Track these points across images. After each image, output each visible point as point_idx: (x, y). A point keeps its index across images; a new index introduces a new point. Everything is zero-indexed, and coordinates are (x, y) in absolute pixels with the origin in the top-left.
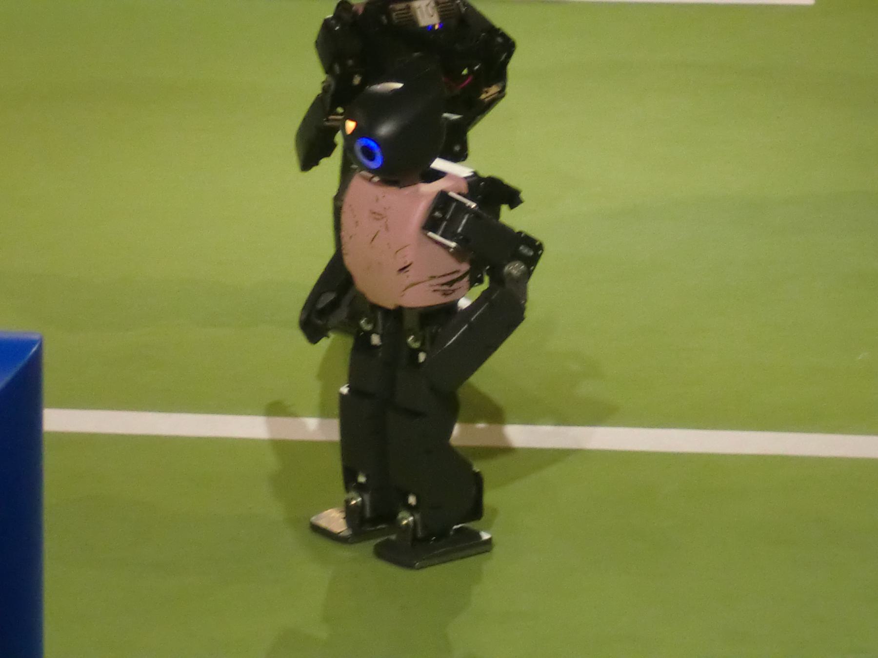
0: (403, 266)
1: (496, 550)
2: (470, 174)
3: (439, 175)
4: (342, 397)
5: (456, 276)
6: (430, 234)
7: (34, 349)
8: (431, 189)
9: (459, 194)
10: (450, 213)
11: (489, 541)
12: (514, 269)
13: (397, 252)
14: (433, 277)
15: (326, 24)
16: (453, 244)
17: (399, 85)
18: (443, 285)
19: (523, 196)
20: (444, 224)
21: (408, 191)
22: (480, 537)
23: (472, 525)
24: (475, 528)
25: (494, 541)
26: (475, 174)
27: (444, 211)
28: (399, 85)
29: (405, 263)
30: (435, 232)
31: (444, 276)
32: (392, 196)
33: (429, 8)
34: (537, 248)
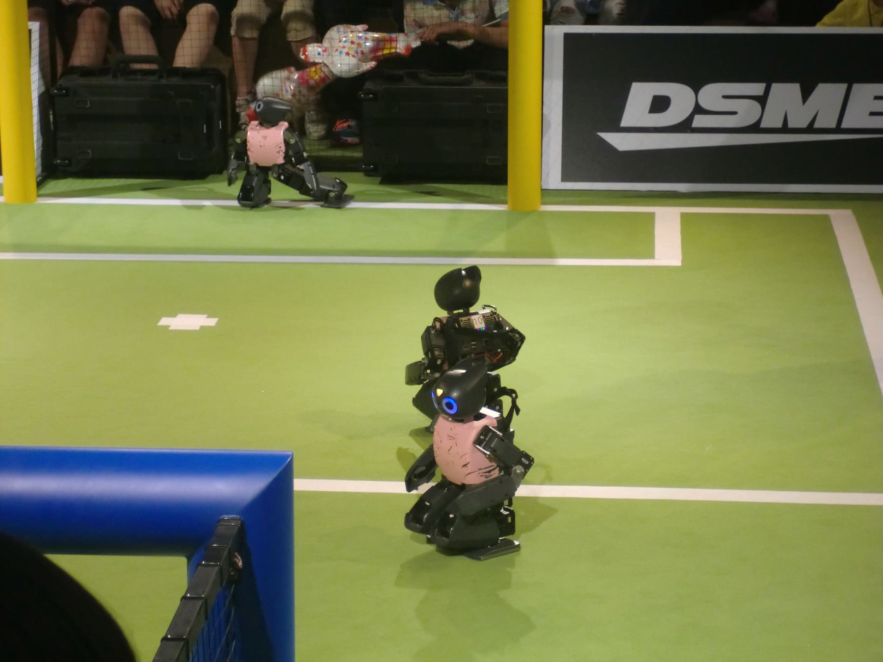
0: (465, 464)
1: (522, 550)
3: (483, 416)
5: (491, 468)
6: (477, 446)
8: (479, 424)
9: (493, 427)
10: (489, 437)
11: (518, 546)
12: (519, 469)
14: (480, 469)
15: (428, 330)
16: (488, 453)
17: (464, 371)
18: (485, 473)
20: (485, 442)
21: (466, 425)
22: (514, 543)
23: (509, 537)
24: (511, 539)
25: (521, 546)
27: (486, 436)
28: (464, 371)
29: (466, 462)
30: (480, 446)
31: (486, 468)
32: (459, 427)
34: (531, 460)
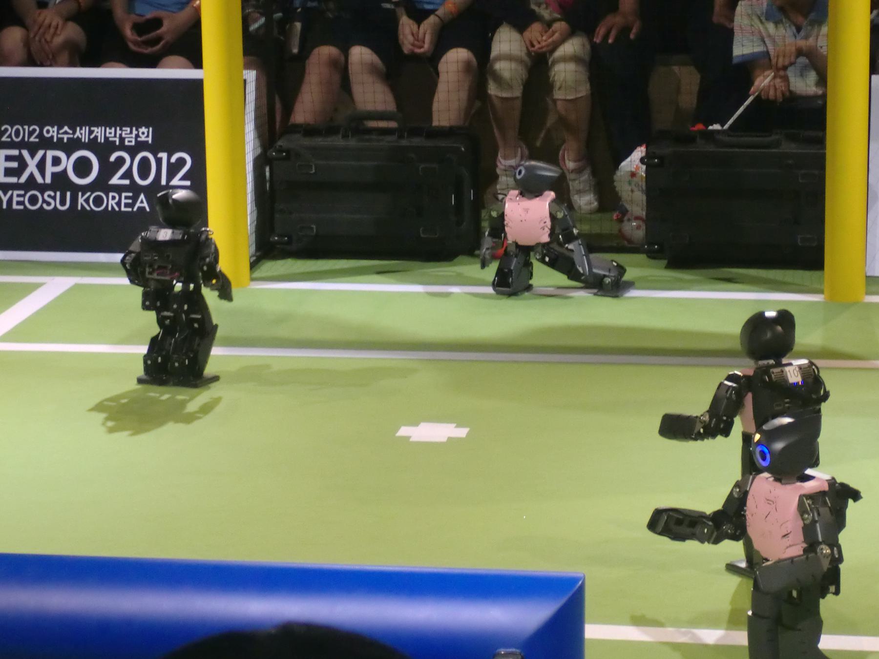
0: (786, 533)
2: (830, 478)
4: (749, 616)
7: (580, 583)
13: (782, 525)
19: (862, 494)
26: (833, 479)
33: (795, 372)
